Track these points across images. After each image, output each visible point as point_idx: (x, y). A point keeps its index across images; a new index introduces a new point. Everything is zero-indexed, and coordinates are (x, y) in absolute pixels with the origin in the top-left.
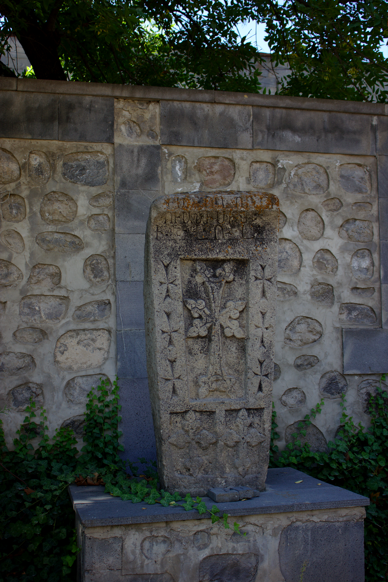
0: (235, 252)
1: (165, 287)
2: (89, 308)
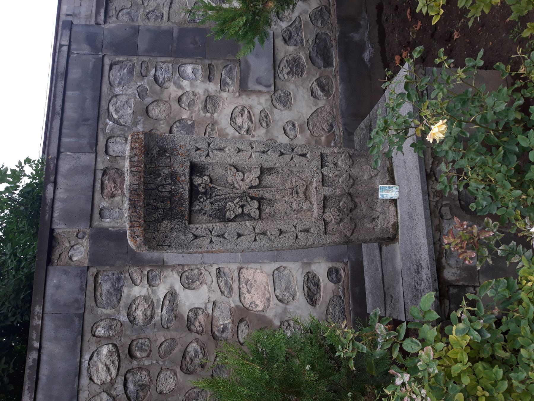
0: (183, 174)
1: (214, 239)
2: (222, 285)
